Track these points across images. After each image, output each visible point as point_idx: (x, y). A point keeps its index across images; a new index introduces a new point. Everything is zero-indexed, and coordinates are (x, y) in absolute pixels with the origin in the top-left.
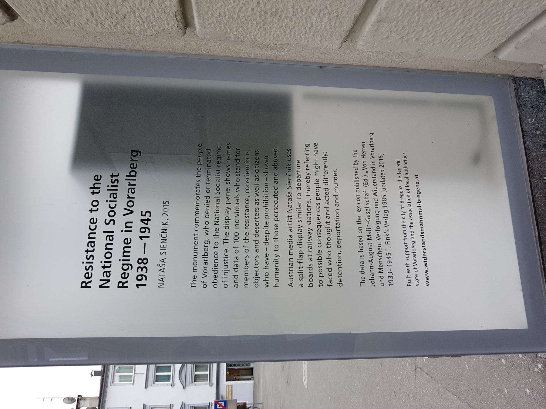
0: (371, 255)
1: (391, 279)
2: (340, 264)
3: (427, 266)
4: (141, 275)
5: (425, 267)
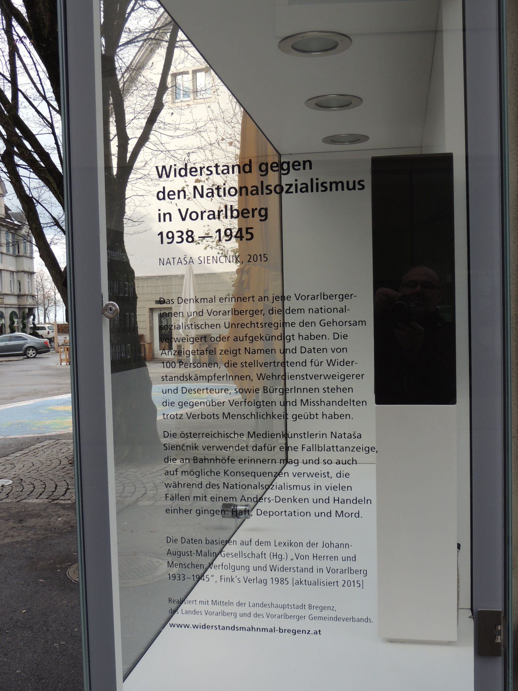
0: (177, 554)
1: (177, 578)
2: (296, 514)
3: (194, 628)
4: (173, 237)
5: (193, 625)
